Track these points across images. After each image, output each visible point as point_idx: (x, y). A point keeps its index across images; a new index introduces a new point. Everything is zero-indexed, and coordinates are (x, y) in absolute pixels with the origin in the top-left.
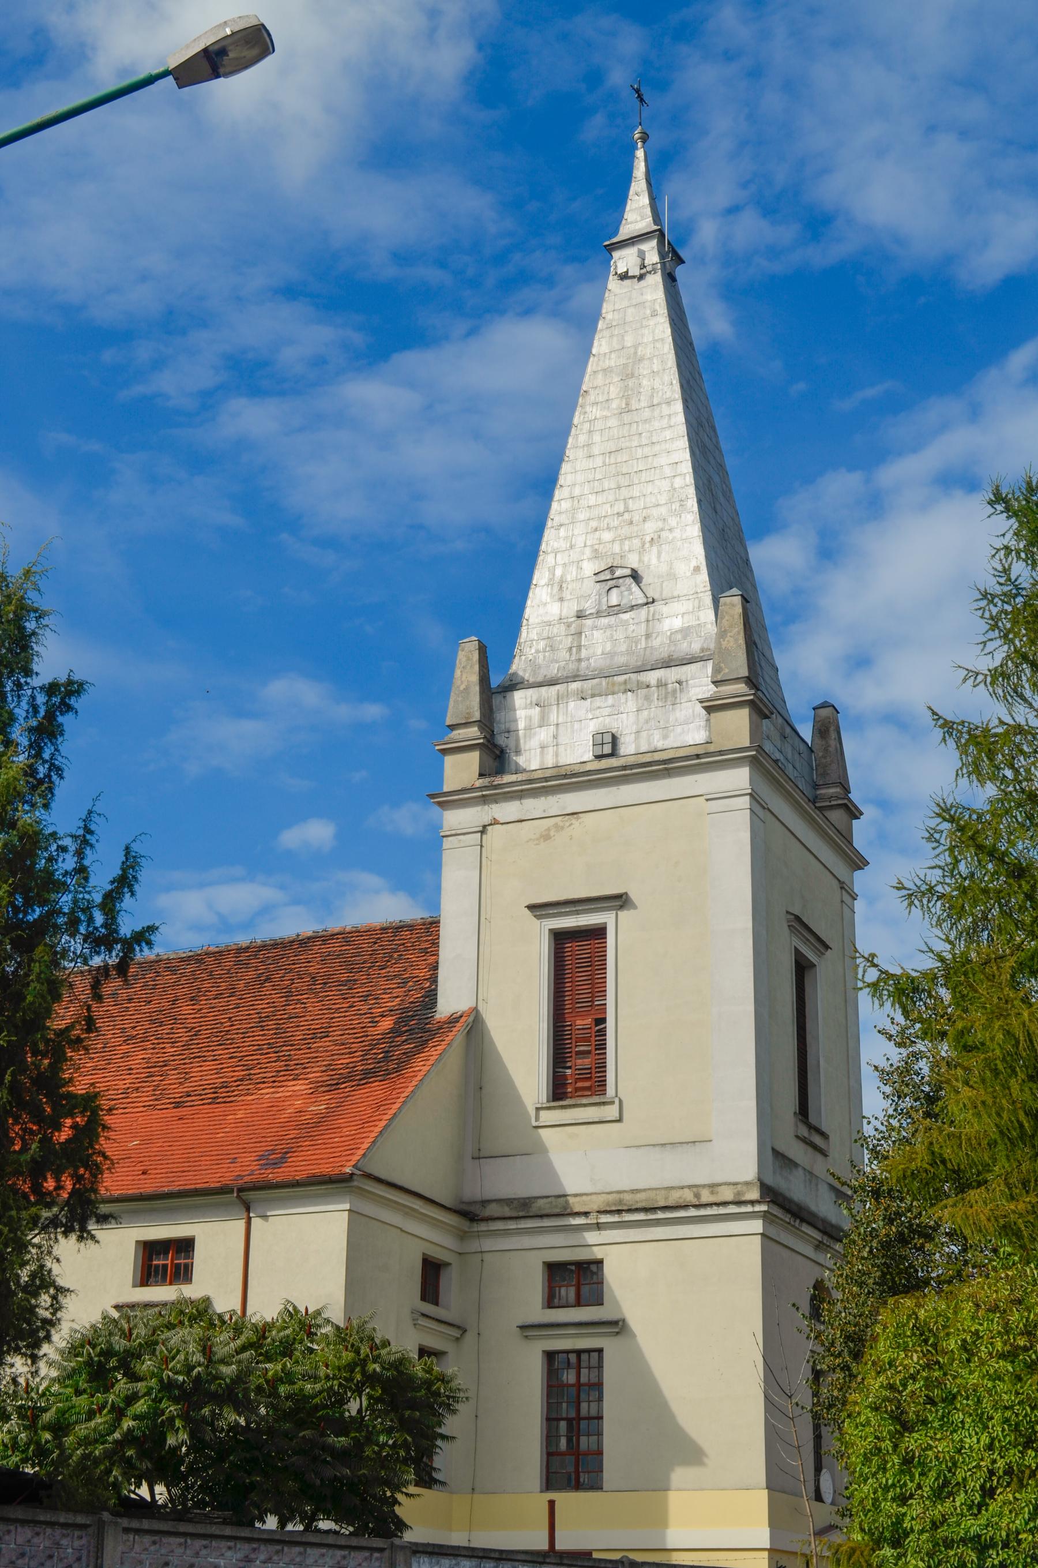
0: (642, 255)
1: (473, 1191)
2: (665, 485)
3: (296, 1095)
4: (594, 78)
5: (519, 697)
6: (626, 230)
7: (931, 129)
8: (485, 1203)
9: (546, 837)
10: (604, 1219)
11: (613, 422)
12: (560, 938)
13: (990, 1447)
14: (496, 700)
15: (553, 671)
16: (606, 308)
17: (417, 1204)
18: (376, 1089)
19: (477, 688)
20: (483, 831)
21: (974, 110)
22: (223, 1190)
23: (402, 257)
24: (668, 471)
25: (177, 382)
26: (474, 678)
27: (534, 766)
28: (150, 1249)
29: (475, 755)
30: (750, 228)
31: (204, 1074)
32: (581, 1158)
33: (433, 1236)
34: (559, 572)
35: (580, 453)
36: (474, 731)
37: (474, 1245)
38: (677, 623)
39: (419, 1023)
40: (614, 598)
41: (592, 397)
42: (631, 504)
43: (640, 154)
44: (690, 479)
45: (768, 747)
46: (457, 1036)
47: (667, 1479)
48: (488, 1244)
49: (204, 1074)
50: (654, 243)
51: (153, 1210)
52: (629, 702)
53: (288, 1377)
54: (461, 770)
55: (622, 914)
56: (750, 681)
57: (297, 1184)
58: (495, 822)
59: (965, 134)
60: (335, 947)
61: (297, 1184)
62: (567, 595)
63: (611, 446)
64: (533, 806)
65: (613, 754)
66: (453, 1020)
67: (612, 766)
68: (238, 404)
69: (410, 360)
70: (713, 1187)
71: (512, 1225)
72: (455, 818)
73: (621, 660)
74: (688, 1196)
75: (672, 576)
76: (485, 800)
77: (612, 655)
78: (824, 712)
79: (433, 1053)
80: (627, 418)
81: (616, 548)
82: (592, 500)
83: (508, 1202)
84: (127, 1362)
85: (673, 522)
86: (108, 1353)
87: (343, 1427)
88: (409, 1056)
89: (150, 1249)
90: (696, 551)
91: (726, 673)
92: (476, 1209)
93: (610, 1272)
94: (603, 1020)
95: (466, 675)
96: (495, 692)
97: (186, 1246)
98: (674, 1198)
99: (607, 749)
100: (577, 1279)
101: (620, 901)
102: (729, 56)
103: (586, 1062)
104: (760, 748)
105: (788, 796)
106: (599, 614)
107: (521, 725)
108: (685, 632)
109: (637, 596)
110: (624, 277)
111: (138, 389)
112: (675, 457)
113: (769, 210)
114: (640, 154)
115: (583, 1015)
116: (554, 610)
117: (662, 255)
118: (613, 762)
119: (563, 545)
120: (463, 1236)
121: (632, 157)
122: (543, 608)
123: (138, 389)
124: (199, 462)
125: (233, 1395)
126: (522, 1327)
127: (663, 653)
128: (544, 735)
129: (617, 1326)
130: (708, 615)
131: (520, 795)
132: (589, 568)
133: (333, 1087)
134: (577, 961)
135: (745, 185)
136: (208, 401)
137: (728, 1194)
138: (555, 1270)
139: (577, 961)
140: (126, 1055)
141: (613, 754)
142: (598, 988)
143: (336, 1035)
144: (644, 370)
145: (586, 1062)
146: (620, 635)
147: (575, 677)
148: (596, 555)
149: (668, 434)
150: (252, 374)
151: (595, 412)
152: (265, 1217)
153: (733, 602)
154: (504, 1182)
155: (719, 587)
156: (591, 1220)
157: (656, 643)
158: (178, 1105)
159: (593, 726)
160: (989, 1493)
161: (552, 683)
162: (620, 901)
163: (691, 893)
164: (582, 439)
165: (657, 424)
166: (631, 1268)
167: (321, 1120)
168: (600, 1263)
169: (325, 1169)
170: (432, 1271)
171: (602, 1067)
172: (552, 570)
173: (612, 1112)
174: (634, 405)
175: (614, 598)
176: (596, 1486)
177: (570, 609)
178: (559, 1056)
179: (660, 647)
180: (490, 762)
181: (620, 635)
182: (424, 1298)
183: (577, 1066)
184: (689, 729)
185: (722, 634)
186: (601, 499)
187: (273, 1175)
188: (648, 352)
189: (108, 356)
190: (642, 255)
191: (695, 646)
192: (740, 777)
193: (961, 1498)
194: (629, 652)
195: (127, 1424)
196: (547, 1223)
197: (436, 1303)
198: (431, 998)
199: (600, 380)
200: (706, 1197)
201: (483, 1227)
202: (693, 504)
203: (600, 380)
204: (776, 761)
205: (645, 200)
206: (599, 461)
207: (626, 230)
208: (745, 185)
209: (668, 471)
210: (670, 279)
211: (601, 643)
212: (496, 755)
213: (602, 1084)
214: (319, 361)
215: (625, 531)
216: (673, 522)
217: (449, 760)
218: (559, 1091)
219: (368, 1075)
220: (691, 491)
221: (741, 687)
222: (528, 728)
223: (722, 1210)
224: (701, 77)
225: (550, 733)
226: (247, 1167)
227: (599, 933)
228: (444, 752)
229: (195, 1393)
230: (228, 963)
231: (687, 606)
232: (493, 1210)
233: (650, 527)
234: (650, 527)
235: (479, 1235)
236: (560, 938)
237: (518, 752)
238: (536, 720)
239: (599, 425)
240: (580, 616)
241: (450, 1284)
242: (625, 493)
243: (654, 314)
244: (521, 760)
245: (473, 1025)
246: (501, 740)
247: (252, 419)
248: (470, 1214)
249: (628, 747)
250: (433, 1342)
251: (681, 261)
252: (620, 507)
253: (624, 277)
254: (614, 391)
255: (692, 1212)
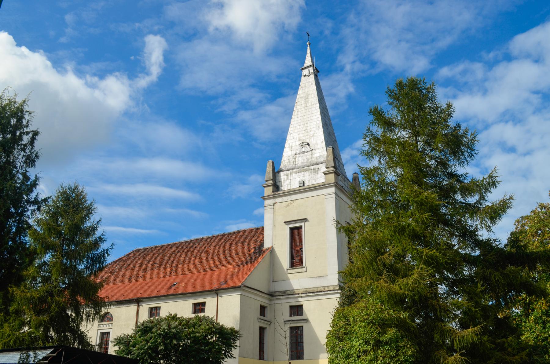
0: (309, 71)
1: (272, 290)
2: (315, 123)
3: (231, 268)
4: (321, 33)
5: (282, 174)
6: (305, 65)
7: (400, 41)
8: (275, 292)
9: (288, 206)
10: (303, 295)
11: (303, 109)
12: (292, 229)
13: (359, 345)
14: (277, 174)
15: (290, 167)
16: (301, 83)
17: (258, 293)
18: (249, 266)
19: (272, 172)
20: (274, 205)
21: (410, 36)
22: (212, 291)
23: (279, 76)
24: (316, 120)
25: (228, 108)
26: (271, 170)
27: (285, 189)
28: (195, 305)
29: (271, 187)
30: (358, 66)
31: (210, 264)
32: (297, 281)
33: (264, 301)
34: (291, 144)
35: (296, 117)
36: (271, 182)
37: (273, 302)
38: (318, 155)
39: (259, 250)
40: (303, 150)
41: (298, 104)
42: (307, 128)
43: (309, 48)
44: (321, 121)
45: (340, 183)
46: (268, 253)
47: (319, 356)
48: (276, 302)
49: (210, 264)
50: (312, 68)
51: (196, 296)
52: (307, 173)
53: (193, 332)
54: (269, 191)
55: (306, 223)
56: (334, 167)
57: (228, 289)
58: (276, 203)
59: (407, 42)
60: (242, 234)
61: (228, 289)
62: (293, 149)
63: (303, 115)
64: (285, 199)
65: (304, 185)
66: (267, 249)
67: (303, 188)
68: (242, 112)
69: (281, 100)
70: (328, 287)
71: (281, 297)
72: (267, 202)
73: (305, 164)
74: (322, 289)
75: (317, 144)
76: (274, 198)
77: (303, 163)
78: (355, 175)
79: (262, 257)
80: (306, 108)
81: (304, 138)
82: (298, 127)
83: (281, 292)
84: (151, 328)
85: (317, 131)
86: (147, 327)
87: (208, 344)
88: (257, 258)
89: (195, 305)
90: (322, 138)
91: (329, 165)
92: (273, 294)
93: (304, 308)
94: (302, 248)
95: (269, 169)
96: (276, 172)
97: (203, 304)
98: (319, 289)
99: (302, 185)
100: (297, 310)
101: (305, 220)
102: (352, 26)
103: (298, 258)
104: (337, 183)
105: (345, 194)
106: (300, 153)
107: (282, 180)
108: (320, 157)
109: (309, 149)
110: (305, 76)
111: (219, 110)
112: (317, 116)
113: (362, 62)
114: (309, 48)
115: (298, 247)
116: (290, 153)
117: (314, 70)
118: (303, 187)
119: (292, 138)
120: (270, 300)
121: (307, 49)
122: (287, 153)
123: (219, 110)
124: (233, 126)
125: (176, 336)
126: (285, 321)
127: (315, 162)
128: (287, 182)
129: (306, 320)
130: (325, 153)
131: (282, 196)
132: (298, 143)
133: (239, 266)
134: (296, 234)
135: (356, 56)
136: (235, 111)
137: (331, 288)
138: (292, 307)
139: (296, 234)
140: (193, 260)
141: (304, 185)
142: (301, 241)
143: (241, 254)
144: (310, 97)
145: (298, 258)
146: (305, 158)
147: (295, 168)
148: (299, 140)
149: (315, 111)
150: (245, 105)
151: (299, 107)
152: (221, 297)
153: (330, 149)
154: (279, 287)
155: (327, 145)
156: (300, 295)
157: (313, 160)
158: (204, 271)
159: (299, 180)
160: (359, 357)
161: (289, 170)
162: (305, 220)
163: (322, 218)
164: (296, 113)
165: (313, 109)
166: (310, 307)
167: (235, 274)
168: (301, 306)
169: (235, 285)
170: (263, 309)
171: (302, 259)
172: (289, 144)
173: (304, 270)
174: (308, 105)
175: (303, 150)
176: (302, 359)
177: (293, 153)
178: (292, 256)
179: (314, 160)
180: (275, 189)
181: (305, 158)
182: (261, 315)
183: (296, 260)
184: (321, 179)
185: (328, 156)
186: (300, 127)
187: (223, 287)
188: (311, 93)
189: (213, 102)
190: (309, 71)
191: (322, 160)
192: (332, 190)
193: (353, 358)
194: (307, 162)
195: (149, 344)
196: (289, 296)
197: (264, 316)
198: (263, 244)
199: (300, 100)
200: (326, 289)
201: (275, 298)
202: (321, 127)
203: (300, 100)
204: (342, 187)
205: (310, 58)
206: (300, 118)
207: (305, 65)
208: (356, 56)
209: (316, 120)
210: (316, 76)
211: (301, 160)
212: (276, 187)
213: (302, 263)
214: (260, 101)
215: (306, 134)
216: (317, 131)
217: (265, 189)
218: (292, 265)
219: (247, 263)
220: (321, 124)
221: (332, 169)
222: (284, 181)
223: (330, 292)
224: (346, 31)
225: (289, 182)
226: (217, 285)
227: (301, 228)
228: (264, 187)
229: (167, 336)
230: (218, 238)
231: (321, 150)
232: (277, 294)
233: (312, 133)
234: (312, 133)
235: (274, 300)
236: (292, 229)
237: (282, 186)
238: (286, 179)
239: (300, 110)
240: (296, 154)
241: (268, 312)
242: (306, 125)
243: (312, 84)
244: (282, 188)
245: (272, 250)
246: (278, 184)
247: (245, 116)
248: (272, 295)
249: (307, 184)
250: (263, 325)
251: (318, 72)
252: (305, 129)
253: (305, 76)
254: (303, 102)
255: (323, 293)
